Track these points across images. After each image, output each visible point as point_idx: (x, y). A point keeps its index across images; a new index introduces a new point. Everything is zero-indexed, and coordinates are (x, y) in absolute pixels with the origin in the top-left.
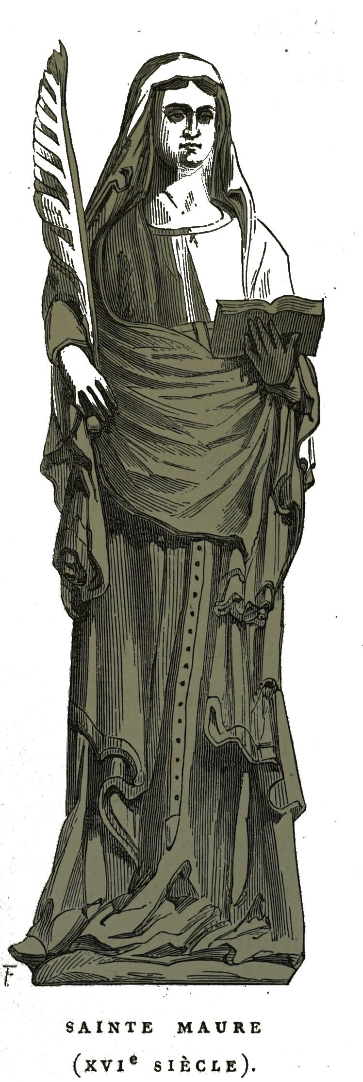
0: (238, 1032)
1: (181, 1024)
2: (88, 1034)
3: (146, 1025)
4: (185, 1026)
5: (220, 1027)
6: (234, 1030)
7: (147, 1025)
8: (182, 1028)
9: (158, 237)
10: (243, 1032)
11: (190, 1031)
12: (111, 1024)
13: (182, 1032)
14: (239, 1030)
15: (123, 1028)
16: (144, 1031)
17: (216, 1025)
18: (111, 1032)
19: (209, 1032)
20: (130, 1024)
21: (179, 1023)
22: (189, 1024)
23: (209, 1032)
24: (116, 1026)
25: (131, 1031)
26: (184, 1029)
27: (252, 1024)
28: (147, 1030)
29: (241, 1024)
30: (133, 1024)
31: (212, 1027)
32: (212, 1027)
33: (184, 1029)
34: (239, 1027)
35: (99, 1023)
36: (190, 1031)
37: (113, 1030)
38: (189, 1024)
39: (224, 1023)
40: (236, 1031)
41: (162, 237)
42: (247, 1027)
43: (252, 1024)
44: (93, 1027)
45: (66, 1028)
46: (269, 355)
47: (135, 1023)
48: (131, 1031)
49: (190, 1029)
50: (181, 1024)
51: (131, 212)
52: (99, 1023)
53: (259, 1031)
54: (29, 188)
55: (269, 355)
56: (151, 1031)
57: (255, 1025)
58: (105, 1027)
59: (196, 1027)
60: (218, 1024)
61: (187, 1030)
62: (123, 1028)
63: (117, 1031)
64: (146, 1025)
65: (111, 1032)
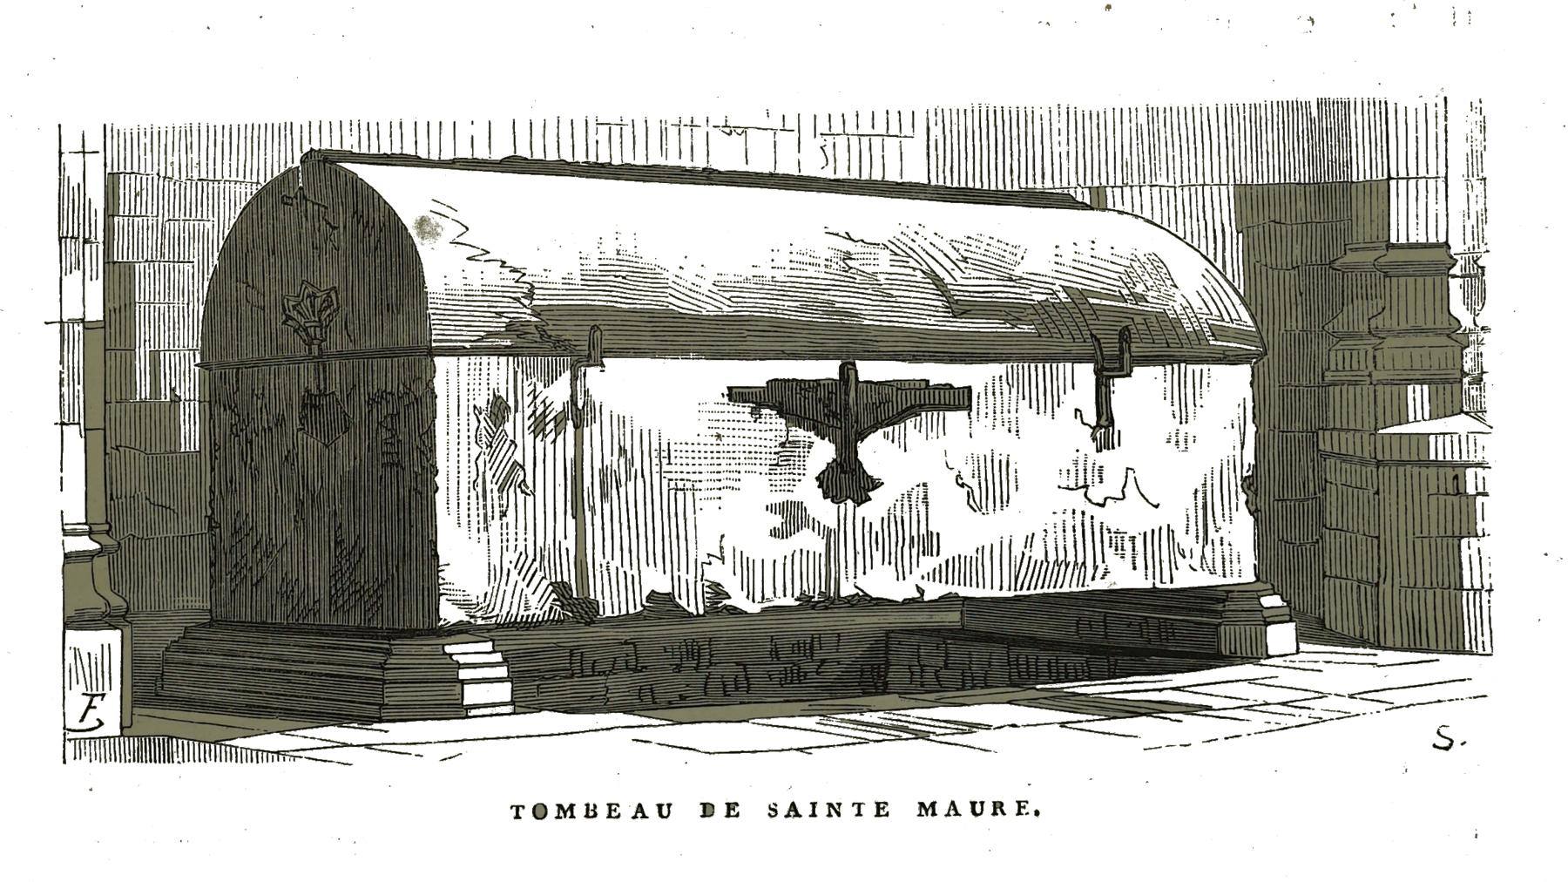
0: (997, 814)
1: (922, 805)
2: (797, 818)
3: (731, 806)
4: (566, 809)
5: (591, 812)
6: (875, 813)
7: (732, 806)
8: (561, 812)
9: (138, 447)
10: (1003, 813)
11: (572, 816)
12: (830, 805)
13: (561, 818)
14: (998, 811)
15: (848, 811)
16: (728, 815)
17: (970, 806)
18: (830, 815)
19: (800, 816)
20: (518, 807)
21: (557, 805)
22: (933, 804)
23: (960, 815)
24: (836, 807)
25: (859, 814)
26: (565, 813)
27: (610, 805)
28: (614, 814)
29: (1002, 804)
30: (521, 808)
31: (964, 808)
32: (964, 808)
33: (565, 813)
34: (998, 807)
35: (814, 805)
36: (934, 814)
37: (833, 812)
38: (933, 804)
39: (982, 803)
40: (995, 814)
41: (138, 447)
42: (1010, 808)
43: (610, 805)
44: (804, 809)
45: (778, 808)
46: (493, 449)
47: (523, 807)
48: (517, 817)
49: (572, 812)
50: (922, 805)
51: (596, 427)
52: (814, 805)
53: (737, 815)
54: (1202, 406)
55: (493, 449)
56: (618, 816)
57: (882, 806)
58: (822, 810)
59: (942, 808)
60: (660, 806)
61: (930, 812)
62: (848, 811)
63: (839, 814)
64: (731, 806)
65: (830, 815)
